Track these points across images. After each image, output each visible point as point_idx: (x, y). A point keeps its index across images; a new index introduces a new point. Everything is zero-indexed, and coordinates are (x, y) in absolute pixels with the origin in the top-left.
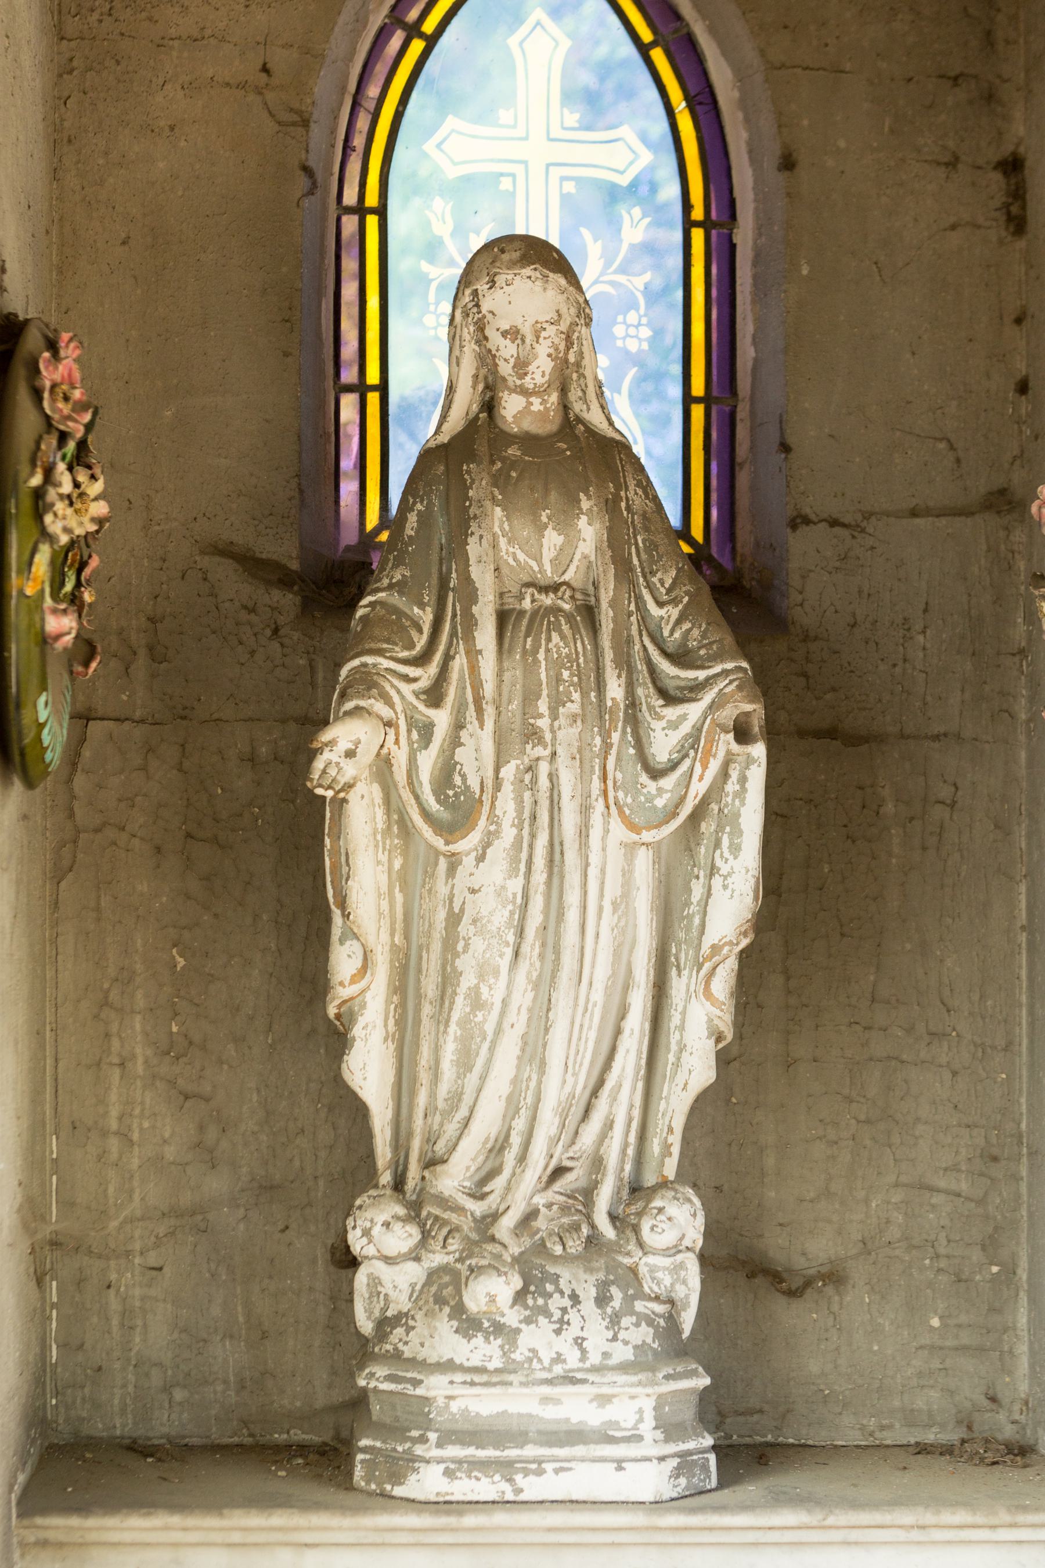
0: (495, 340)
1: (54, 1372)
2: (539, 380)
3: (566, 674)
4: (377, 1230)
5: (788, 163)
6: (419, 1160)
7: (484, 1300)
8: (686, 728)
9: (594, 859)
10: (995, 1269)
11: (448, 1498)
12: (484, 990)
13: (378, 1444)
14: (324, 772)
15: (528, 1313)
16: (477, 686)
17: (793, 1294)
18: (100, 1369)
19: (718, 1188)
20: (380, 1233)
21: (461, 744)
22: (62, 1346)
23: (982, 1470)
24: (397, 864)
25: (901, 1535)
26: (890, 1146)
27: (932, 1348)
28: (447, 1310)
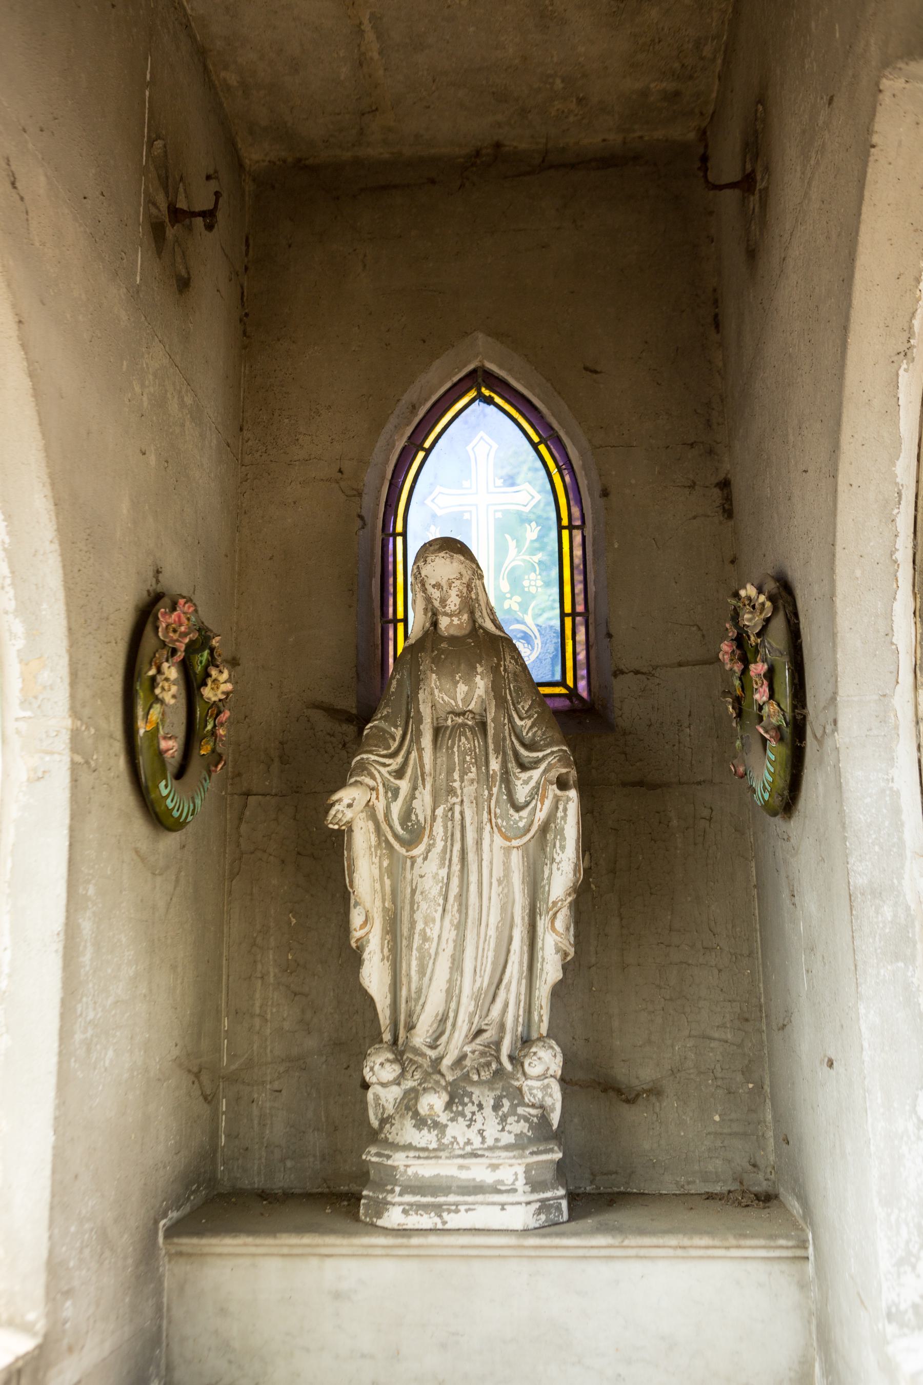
0: (430, 590)
1: (223, 1151)
2: (453, 608)
3: (468, 758)
4: (377, 1067)
5: (605, 493)
6: (405, 1027)
7: (427, 1108)
8: (532, 783)
9: (486, 856)
10: (751, 1086)
11: (405, 1227)
12: (428, 930)
13: (371, 1194)
14: (335, 816)
15: (452, 1115)
16: (422, 767)
17: (630, 1102)
18: (247, 1149)
19: (587, 1040)
20: (380, 1069)
21: (416, 798)
22: (228, 1136)
23: (738, 1210)
24: (386, 863)
25: (671, 1252)
26: (684, 1014)
27: (716, 1134)
28: (410, 1114)
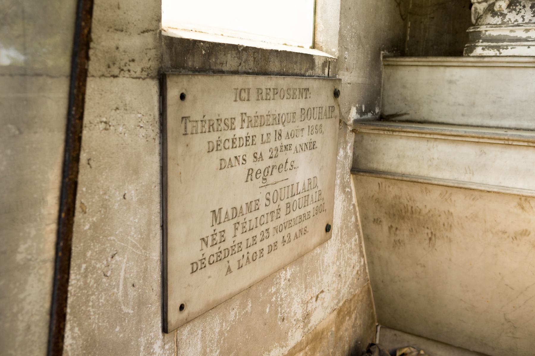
22: (410, 37)
